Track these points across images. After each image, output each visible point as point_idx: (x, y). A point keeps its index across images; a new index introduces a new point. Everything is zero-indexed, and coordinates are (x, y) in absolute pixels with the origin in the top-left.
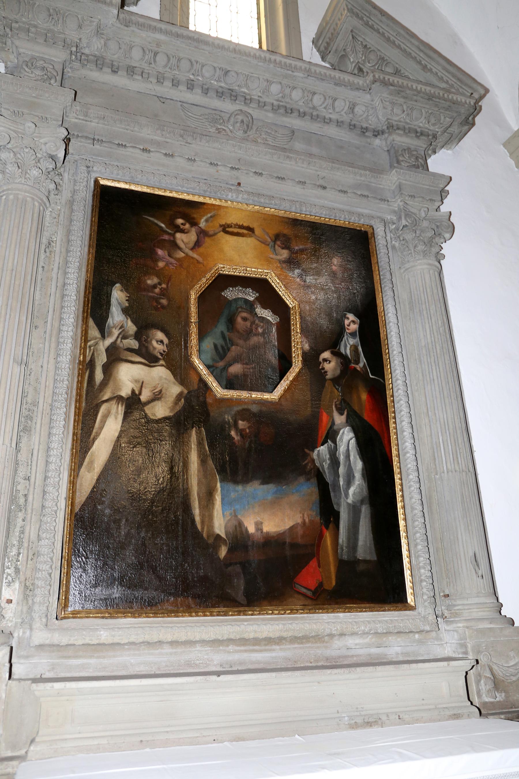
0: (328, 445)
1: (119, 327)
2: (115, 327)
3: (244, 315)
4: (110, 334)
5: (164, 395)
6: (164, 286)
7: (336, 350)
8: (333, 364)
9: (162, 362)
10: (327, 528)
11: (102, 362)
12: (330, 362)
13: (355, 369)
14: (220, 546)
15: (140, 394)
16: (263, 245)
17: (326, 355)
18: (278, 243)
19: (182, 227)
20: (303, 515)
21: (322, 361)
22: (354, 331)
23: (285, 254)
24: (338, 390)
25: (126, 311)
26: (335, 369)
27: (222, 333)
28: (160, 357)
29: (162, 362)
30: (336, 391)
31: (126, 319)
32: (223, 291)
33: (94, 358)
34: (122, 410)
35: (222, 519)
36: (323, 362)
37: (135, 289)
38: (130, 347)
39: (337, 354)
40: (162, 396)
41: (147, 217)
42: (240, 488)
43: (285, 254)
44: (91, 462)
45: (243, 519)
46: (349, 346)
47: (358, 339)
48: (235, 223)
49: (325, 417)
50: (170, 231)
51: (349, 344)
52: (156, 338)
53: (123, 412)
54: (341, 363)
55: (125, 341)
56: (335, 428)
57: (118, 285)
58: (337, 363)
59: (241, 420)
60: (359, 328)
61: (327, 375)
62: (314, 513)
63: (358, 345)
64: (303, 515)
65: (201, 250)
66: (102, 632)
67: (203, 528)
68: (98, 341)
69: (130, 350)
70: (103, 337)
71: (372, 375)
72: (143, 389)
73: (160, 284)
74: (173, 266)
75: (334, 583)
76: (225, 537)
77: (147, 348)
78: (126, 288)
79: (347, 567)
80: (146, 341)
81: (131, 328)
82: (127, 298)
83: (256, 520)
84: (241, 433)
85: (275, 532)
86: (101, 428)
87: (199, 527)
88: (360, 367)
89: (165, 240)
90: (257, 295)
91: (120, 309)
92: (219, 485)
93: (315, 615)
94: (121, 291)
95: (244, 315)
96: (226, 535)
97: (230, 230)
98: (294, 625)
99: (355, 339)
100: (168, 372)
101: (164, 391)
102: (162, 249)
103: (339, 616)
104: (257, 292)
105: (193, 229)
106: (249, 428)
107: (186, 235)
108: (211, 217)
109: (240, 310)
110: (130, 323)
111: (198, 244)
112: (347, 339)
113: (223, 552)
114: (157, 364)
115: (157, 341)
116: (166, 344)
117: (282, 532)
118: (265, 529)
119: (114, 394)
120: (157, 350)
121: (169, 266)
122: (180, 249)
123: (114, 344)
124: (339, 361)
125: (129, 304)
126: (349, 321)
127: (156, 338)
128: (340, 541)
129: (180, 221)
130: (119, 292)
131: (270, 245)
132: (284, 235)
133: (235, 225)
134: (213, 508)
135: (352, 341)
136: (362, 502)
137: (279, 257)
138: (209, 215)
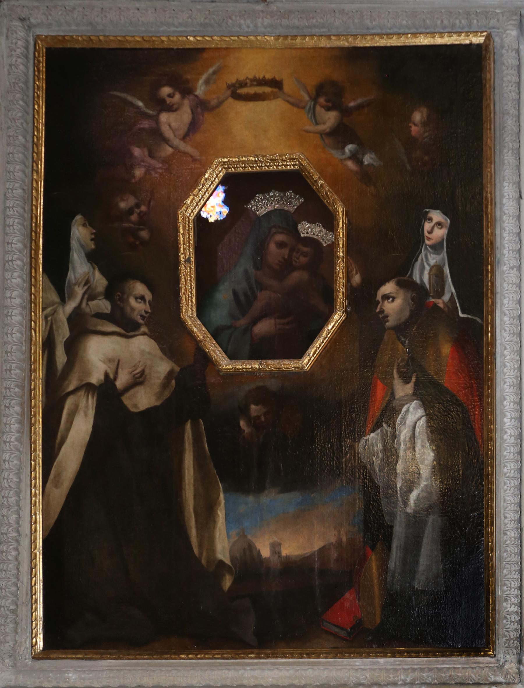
0: (382, 431)
1: (83, 283)
2: (78, 283)
3: (280, 237)
4: (72, 295)
5: (148, 376)
6: (143, 208)
7: (406, 278)
8: (398, 302)
9: (144, 329)
10: (373, 548)
11: (63, 338)
12: (394, 299)
13: (435, 305)
14: (224, 575)
15: (115, 378)
16: (295, 110)
17: (389, 288)
18: (322, 100)
19: (169, 100)
20: (339, 532)
21: (380, 300)
22: (439, 240)
23: (331, 118)
24: (403, 343)
25: (92, 257)
26: (401, 310)
27: (246, 272)
28: (141, 321)
29: (144, 329)
30: (401, 346)
31: (92, 269)
32: (248, 202)
33: (54, 336)
34: (93, 403)
35: (226, 542)
36: (383, 301)
37: (103, 220)
38: (100, 311)
39: (407, 284)
40: (145, 378)
41: (118, 94)
42: (251, 499)
43: (331, 118)
44: (58, 475)
45: (254, 540)
46: (427, 268)
47: (444, 254)
48: (251, 76)
49: (380, 390)
50: (151, 112)
51: (429, 265)
52: (134, 293)
53: (95, 405)
54: (413, 299)
55: (92, 303)
56: (395, 403)
57: (79, 218)
58: (405, 300)
59: (254, 404)
60: (448, 234)
61: (388, 321)
62: (356, 528)
63: (444, 265)
64: (339, 532)
65: (198, 137)
66: (70, 675)
67: (201, 553)
68: (57, 307)
69: (100, 316)
70: (63, 300)
71: (463, 313)
72: (120, 370)
73: (138, 206)
74: (156, 173)
75: (378, 620)
76: (230, 564)
77: (122, 310)
78: (90, 221)
79: (396, 601)
80: (121, 299)
81: (100, 281)
82: (93, 237)
83: (271, 541)
84: (253, 422)
85: (298, 556)
86: (68, 430)
87: (196, 551)
88: (443, 302)
89: (144, 129)
90: (302, 200)
91: (83, 255)
92: (222, 496)
93: (346, 661)
94: (84, 225)
95: (280, 237)
96: (232, 561)
97: (243, 91)
98: (310, 671)
99: (439, 254)
100: (153, 343)
101: (147, 371)
102: (138, 147)
103: (378, 662)
104: (301, 196)
105: (186, 102)
106: (265, 414)
107: (175, 113)
108: (214, 73)
109: (274, 230)
110: (98, 274)
111: (194, 126)
112: (426, 257)
113: (227, 582)
114: (137, 333)
115: (136, 298)
116: (149, 302)
117: (308, 554)
118: (285, 552)
119: (82, 381)
120: (136, 313)
121: (150, 174)
122: (166, 141)
123: (77, 310)
124: (409, 295)
125: (95, 244)
126: (432, 224)
127: (134, 293)
128: (392, 565)
129: (166, 90)
130: (81, 229)
131: (308, 107)
132: (334, 84)
133: (252, 80)
134: (214, 527)
135: (433, 259)
136: (429, 510)
137: (321, 128)
138: (211, 70)
